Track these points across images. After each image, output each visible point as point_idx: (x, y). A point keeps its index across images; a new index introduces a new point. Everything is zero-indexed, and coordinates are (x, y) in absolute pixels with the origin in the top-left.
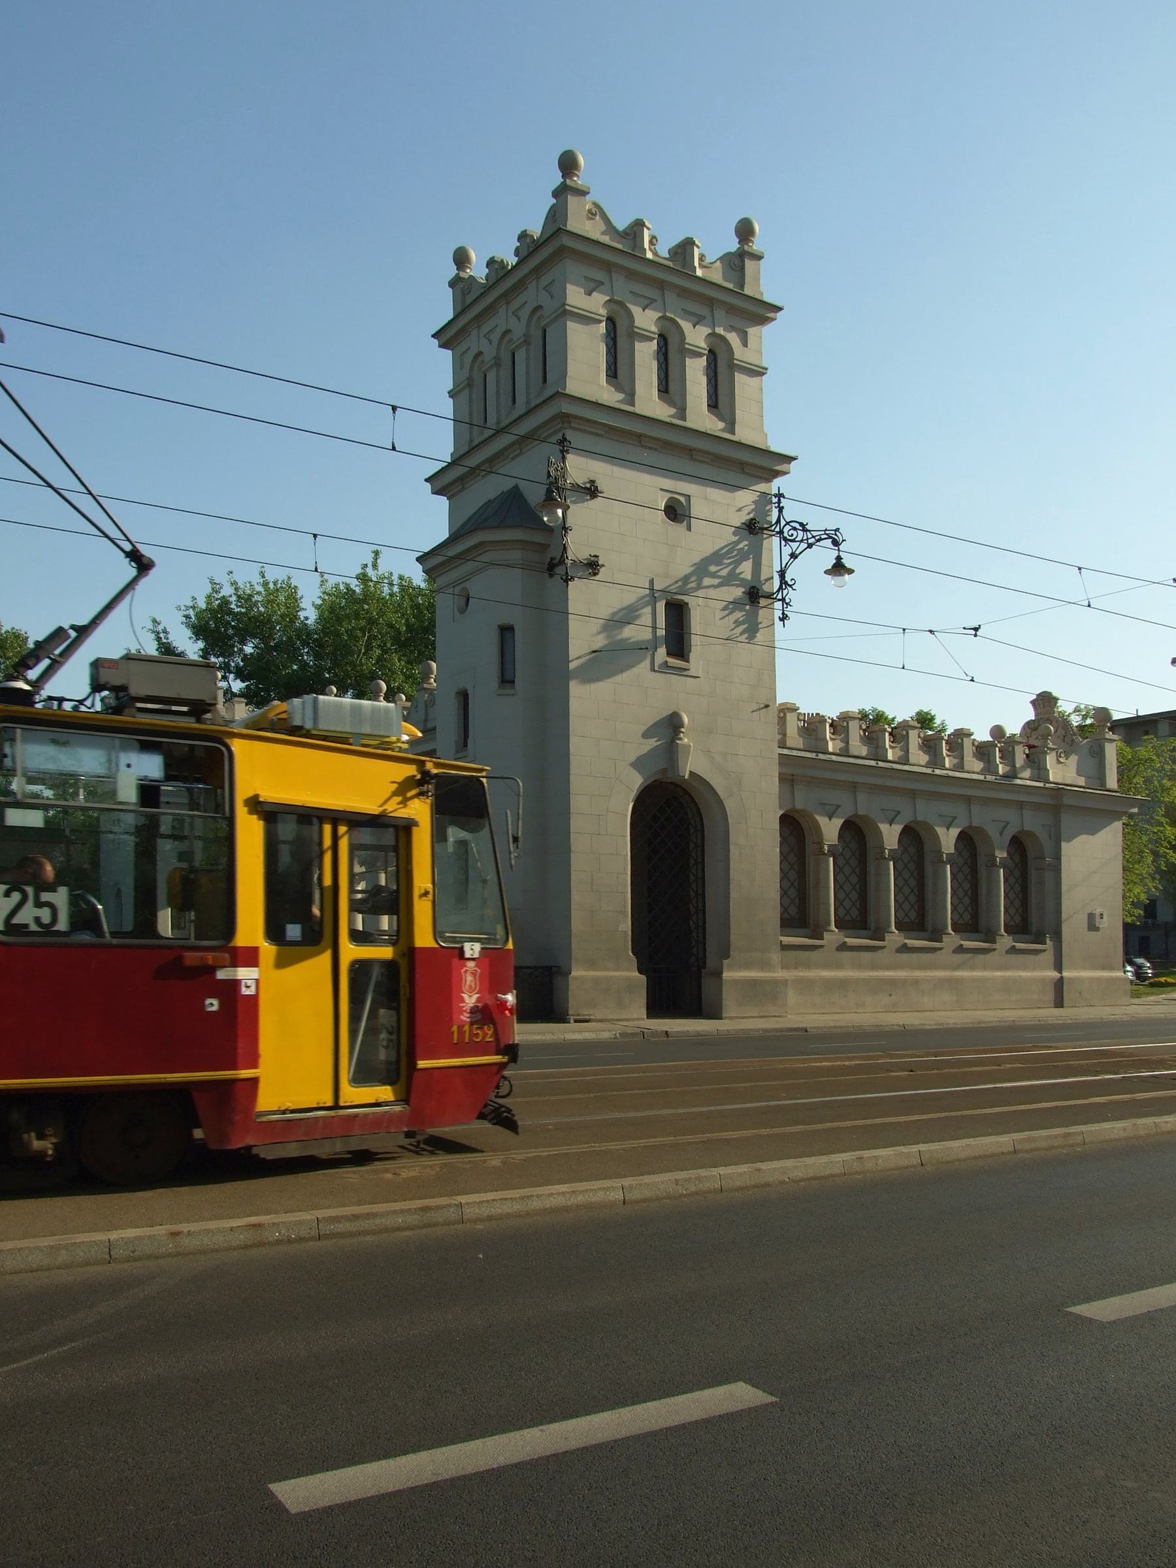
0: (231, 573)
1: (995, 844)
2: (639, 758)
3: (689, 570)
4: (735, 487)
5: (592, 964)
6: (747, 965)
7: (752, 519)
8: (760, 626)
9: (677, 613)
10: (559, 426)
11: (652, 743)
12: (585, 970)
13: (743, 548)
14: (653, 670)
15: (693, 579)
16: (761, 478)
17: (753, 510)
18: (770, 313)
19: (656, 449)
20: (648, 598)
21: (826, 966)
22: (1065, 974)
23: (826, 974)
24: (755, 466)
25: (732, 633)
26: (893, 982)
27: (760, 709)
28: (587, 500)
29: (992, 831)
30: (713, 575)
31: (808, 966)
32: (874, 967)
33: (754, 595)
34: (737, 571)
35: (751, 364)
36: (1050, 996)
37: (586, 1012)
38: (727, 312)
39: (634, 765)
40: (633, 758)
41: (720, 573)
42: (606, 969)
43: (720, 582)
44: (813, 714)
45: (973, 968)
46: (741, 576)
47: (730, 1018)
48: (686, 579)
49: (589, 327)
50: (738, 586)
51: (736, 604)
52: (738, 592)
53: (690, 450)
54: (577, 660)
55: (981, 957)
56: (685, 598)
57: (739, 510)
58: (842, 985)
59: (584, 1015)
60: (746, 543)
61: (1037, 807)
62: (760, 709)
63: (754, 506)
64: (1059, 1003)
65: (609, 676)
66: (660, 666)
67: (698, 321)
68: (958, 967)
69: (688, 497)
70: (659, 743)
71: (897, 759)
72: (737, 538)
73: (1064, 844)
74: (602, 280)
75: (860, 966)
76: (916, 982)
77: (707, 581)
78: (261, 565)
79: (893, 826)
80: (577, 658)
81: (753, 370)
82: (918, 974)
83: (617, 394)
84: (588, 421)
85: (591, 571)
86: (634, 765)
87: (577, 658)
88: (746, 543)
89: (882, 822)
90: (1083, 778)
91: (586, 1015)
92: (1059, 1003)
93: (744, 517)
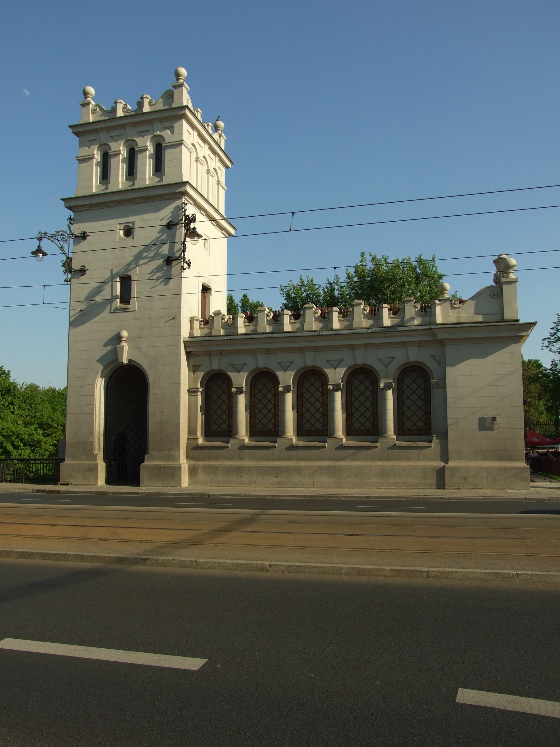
0: (291, 280)
1: (381, 375)
2: (101, 357)
3: (131, 259)
4: (158, 210)
5: (75, 458)
6: (158, 458)
7: (170, 221)
8: (172, 276)
9: (126, 281)
10: (88, 208)
11: (109, 348)
12: (71, 460)
13: (164, 238)
14: (111, 312)
15: (134, 263)
16: (173, 199)
17: (171, 217)
18: (181, 112)
19: (116, 206)
20: (110, 279)
21: (231, 458)
22: (451, 464)
23: (229, 463)
24: (169, 194)
25: (155, 284)
26: (278, 469)
27: (170, 320)
28: (82, 241)
29: (378, 367)
30: (146, 258)
31: (217, 458)
32: (267, 459)
33: (169, 261)
34: (160, 251)
35: (174, 142)
36: (434, 480)
37: (67, 481)
38: (160, 122)
39: (99, 361)
40: (98, 357)
41: (149, 256)
42: (81, 460)
43: (149, 260)
44: (279, 311)
45: (356, 460)
46: (162, 253)
47: (145, 486)
48: (129, 264)
49: (88, 163)
50: (159, 259)
51: (159, 269)
52: (160, 262)
53: (161, 196)
54: (74, 316)
55: (363, 453)
56: (129, 273)
57: (162, 220)
58: (239, 470)
59: (67, 482)
60: (166, 235)
61: (420, 344)
62: (170, 320)
63: (171, 215)
64: (441, 485)
65: (89, 320)
66: (114, 310)
67: (142, 134)
68: (341, 459)
69: (133, 223)
70: (112, 348)
71: (250, 332)
72: (160, 234)
73: (449, 370)
74: (95, 138)
75: (257, 459)
76: (298, 470)
77: (141, 262)
78: (346, 268)
79: (287, 372)
80: (74, 315)
81: (175, 144)
82: (302, 463)
83: (104, 186)
84: (81, 206)
85: (82, 273)
86: (99, 361)
87: (74, 315)
88: (166, 235)
89: (279, 371)
90: (481, 316)
91: (68, 482)
92: (441, 485)
93: (165, 222)
